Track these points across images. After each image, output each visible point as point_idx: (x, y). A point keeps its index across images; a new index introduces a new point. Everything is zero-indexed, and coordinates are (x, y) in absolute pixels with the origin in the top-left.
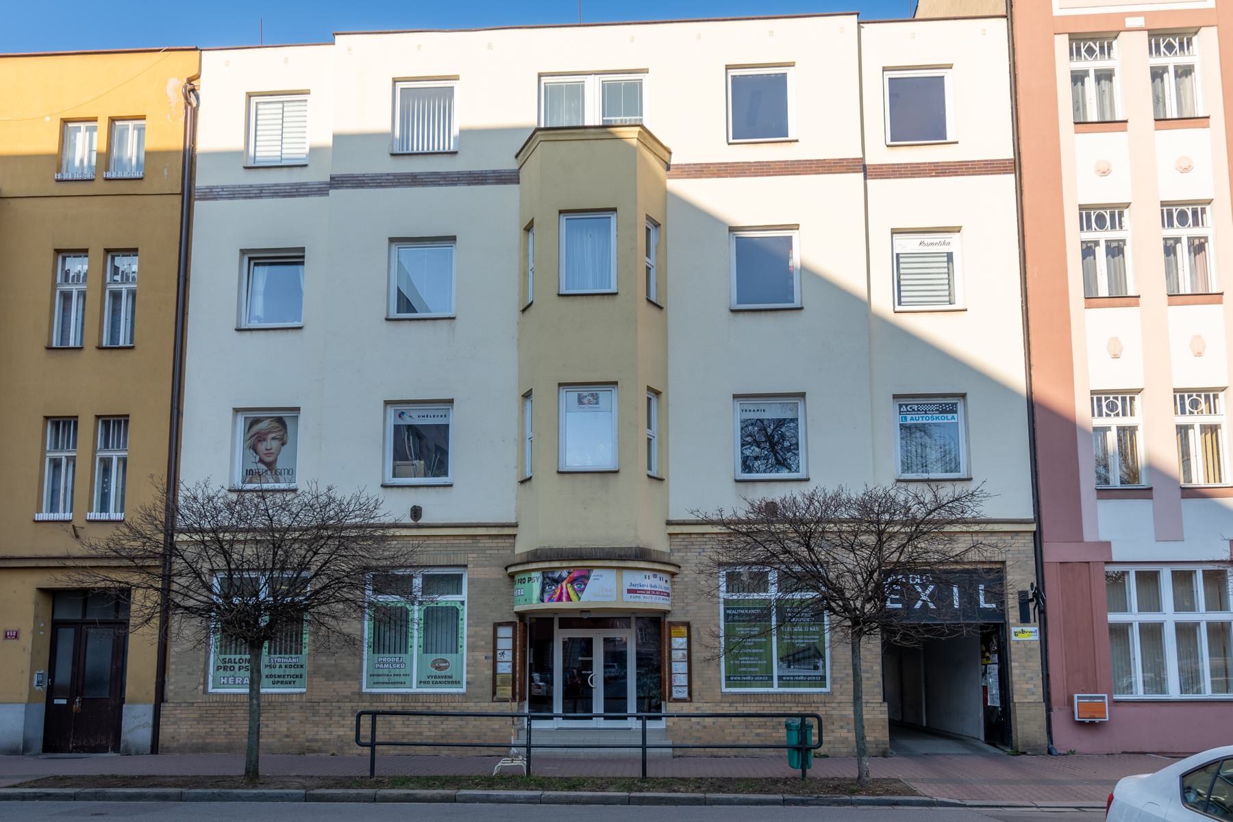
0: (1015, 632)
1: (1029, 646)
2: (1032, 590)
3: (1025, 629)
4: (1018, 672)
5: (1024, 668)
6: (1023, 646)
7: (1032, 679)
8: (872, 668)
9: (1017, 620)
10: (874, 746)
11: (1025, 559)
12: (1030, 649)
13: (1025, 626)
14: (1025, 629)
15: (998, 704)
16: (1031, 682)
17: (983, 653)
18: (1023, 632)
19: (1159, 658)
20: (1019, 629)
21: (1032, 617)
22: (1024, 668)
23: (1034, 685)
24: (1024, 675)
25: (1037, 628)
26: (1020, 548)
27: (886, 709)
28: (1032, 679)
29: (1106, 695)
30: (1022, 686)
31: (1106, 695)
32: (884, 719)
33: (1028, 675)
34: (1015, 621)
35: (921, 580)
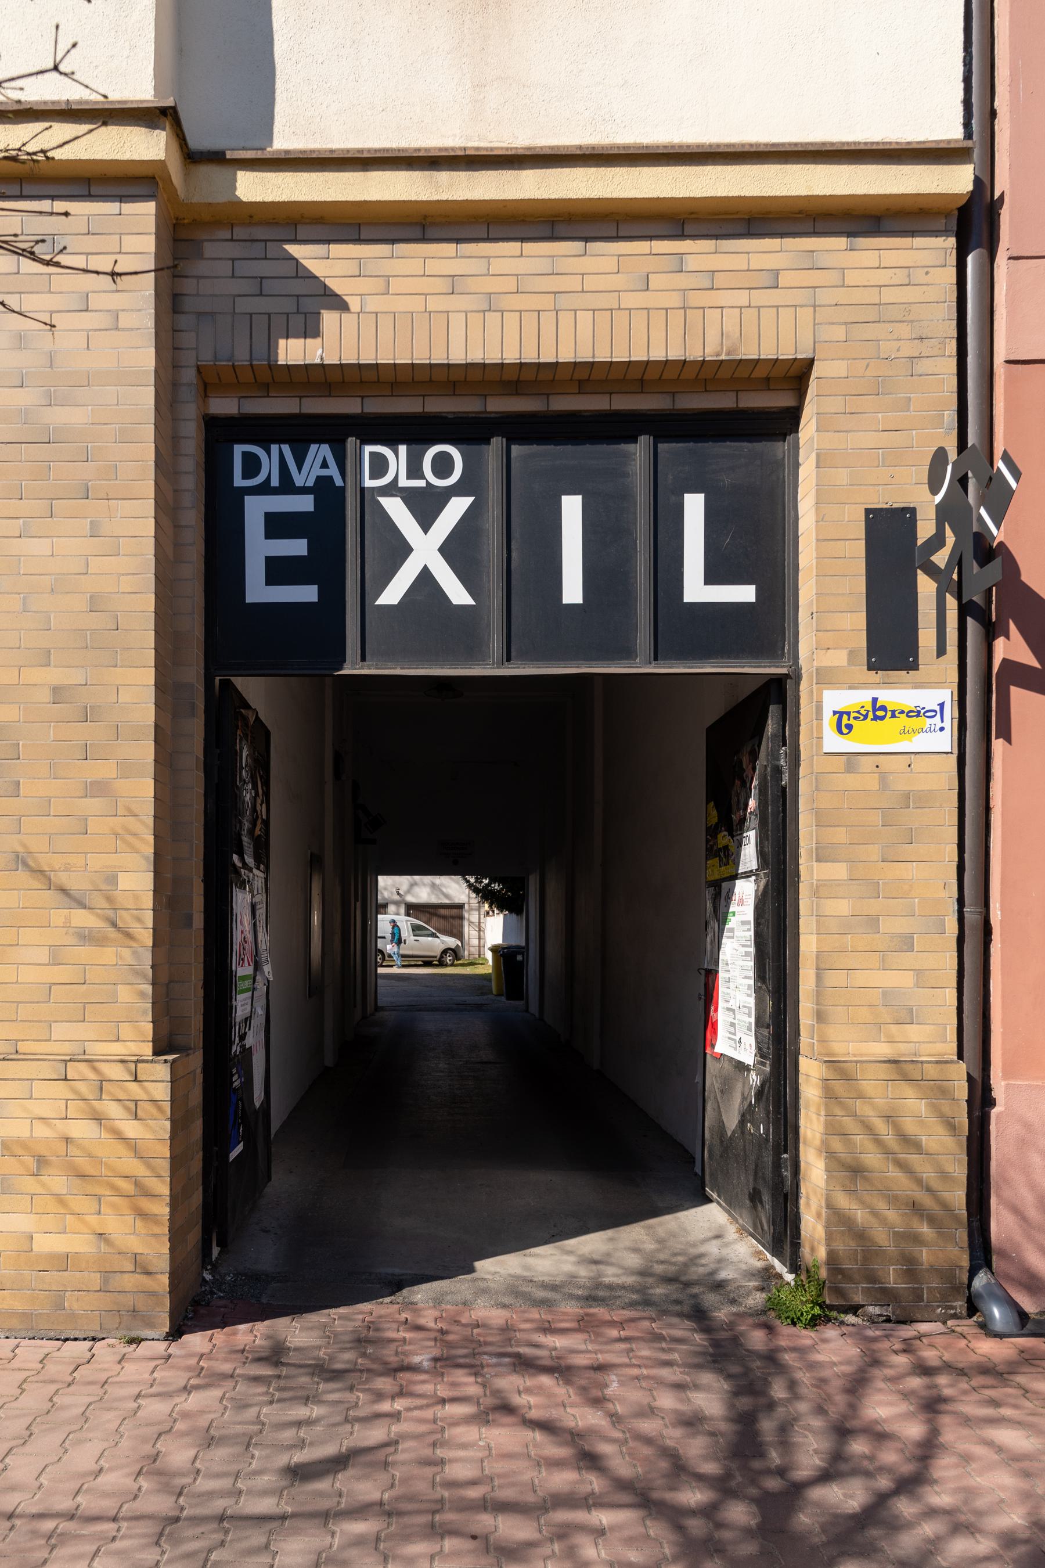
0: (840, 714)
1: (901, 785)
2: (934, 490)
3: (889, 697)
4: (840, 907)
5: (875, 890)
6: (872, 783)
7: (907, 943)
8: (112, 879)
9: (852, 653)
10: (94, 1280)
11: (908, 349)
12: (906, 799)
13: (887, 684)
14: (889, 697)
15: (747, 1055)
16: (907, 959)
17: (712, 832)
18: (878, 711)
19: (242, 1006)
20: (857, 699)
21: (927, 638)
22: (875, 890)
23: (919, 973)
24: (873, 923)
25: (946, 695)
26: (889, 296)
27: (162, 1092)
28: (907, 943)
29: (239, 449)
30: (860, 978)
31: (239, 449)
32: (749, 986)
33: (886, 926)
34: (838, 658)
35: (413, 470)
